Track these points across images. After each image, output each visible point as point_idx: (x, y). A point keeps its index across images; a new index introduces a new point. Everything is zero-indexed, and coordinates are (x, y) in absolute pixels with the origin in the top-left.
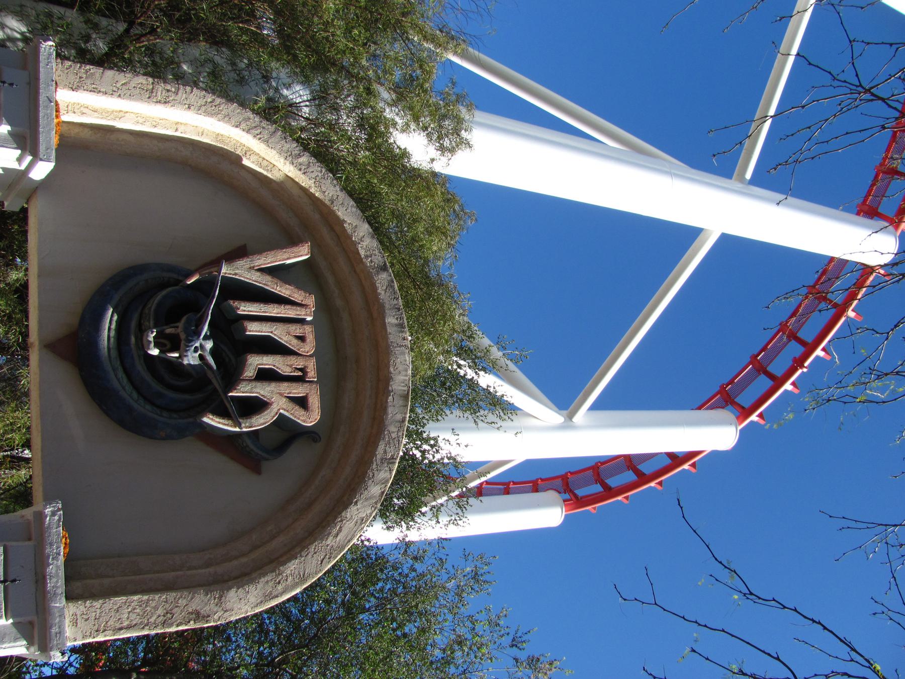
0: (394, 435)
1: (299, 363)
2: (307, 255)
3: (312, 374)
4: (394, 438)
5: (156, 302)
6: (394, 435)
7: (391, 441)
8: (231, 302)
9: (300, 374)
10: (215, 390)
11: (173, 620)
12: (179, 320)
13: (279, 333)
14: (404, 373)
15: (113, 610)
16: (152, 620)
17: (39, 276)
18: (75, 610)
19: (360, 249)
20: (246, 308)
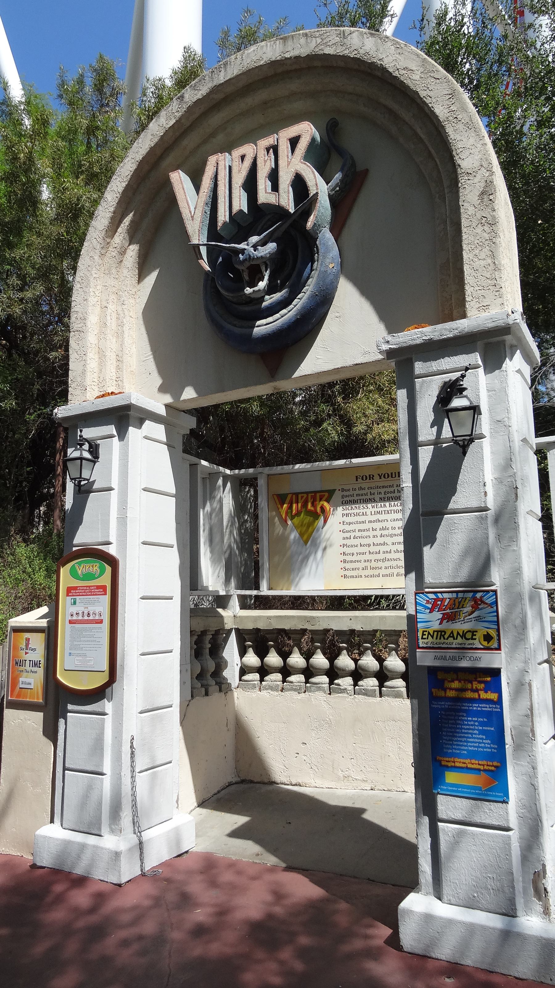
0: (319, 40)
1: (262, 154)
2: (179, 173)
3: (270, 141)
4: (322, 39)
5: (226, 294)
6: (319, 40)
7: (325, 41)
8: (218, 228)
9: (271, 151)
10: (291, 225)
11: (488, 216)
12: (238, 270)
13: (239, 179)
14: (265, 48)
15: (476, 275)
16: (487, 236)
17: (223, 391)
18: (474, 310)
19: (169, 126)
20: (223, 216)
